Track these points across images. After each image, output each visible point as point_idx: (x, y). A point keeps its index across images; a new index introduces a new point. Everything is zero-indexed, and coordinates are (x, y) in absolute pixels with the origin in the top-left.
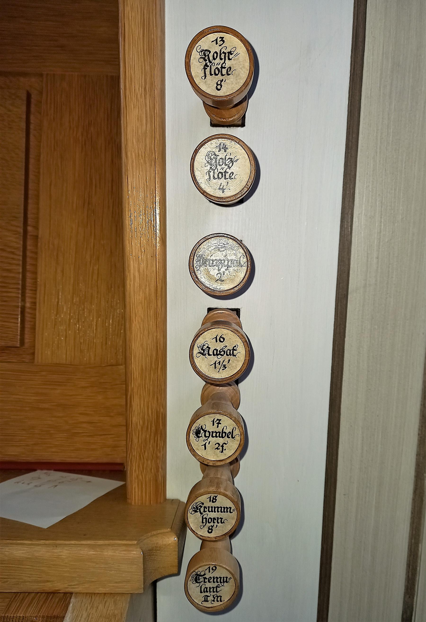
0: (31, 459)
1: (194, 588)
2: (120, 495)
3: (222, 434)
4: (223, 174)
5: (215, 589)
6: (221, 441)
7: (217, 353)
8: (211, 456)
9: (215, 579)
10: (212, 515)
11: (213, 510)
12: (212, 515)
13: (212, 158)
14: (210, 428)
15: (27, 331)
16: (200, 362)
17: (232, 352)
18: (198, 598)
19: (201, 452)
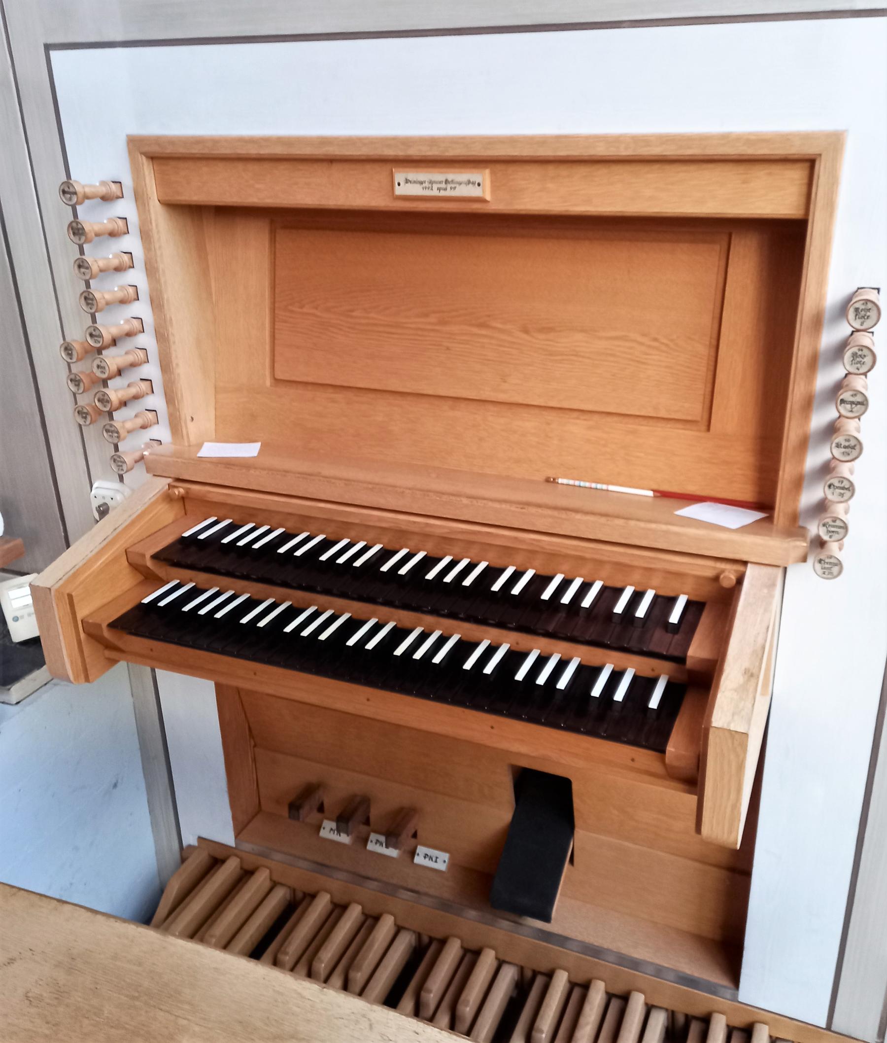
1: (818, 566)
3: (843, 488)
4: (860, 362)
5: (830, 569)
6: (842, 491)
7: (845, 447)
9: (830, 563)
11: (834, 526)
12: (833, 529)
14: (837, 484)
18: (820, 571)
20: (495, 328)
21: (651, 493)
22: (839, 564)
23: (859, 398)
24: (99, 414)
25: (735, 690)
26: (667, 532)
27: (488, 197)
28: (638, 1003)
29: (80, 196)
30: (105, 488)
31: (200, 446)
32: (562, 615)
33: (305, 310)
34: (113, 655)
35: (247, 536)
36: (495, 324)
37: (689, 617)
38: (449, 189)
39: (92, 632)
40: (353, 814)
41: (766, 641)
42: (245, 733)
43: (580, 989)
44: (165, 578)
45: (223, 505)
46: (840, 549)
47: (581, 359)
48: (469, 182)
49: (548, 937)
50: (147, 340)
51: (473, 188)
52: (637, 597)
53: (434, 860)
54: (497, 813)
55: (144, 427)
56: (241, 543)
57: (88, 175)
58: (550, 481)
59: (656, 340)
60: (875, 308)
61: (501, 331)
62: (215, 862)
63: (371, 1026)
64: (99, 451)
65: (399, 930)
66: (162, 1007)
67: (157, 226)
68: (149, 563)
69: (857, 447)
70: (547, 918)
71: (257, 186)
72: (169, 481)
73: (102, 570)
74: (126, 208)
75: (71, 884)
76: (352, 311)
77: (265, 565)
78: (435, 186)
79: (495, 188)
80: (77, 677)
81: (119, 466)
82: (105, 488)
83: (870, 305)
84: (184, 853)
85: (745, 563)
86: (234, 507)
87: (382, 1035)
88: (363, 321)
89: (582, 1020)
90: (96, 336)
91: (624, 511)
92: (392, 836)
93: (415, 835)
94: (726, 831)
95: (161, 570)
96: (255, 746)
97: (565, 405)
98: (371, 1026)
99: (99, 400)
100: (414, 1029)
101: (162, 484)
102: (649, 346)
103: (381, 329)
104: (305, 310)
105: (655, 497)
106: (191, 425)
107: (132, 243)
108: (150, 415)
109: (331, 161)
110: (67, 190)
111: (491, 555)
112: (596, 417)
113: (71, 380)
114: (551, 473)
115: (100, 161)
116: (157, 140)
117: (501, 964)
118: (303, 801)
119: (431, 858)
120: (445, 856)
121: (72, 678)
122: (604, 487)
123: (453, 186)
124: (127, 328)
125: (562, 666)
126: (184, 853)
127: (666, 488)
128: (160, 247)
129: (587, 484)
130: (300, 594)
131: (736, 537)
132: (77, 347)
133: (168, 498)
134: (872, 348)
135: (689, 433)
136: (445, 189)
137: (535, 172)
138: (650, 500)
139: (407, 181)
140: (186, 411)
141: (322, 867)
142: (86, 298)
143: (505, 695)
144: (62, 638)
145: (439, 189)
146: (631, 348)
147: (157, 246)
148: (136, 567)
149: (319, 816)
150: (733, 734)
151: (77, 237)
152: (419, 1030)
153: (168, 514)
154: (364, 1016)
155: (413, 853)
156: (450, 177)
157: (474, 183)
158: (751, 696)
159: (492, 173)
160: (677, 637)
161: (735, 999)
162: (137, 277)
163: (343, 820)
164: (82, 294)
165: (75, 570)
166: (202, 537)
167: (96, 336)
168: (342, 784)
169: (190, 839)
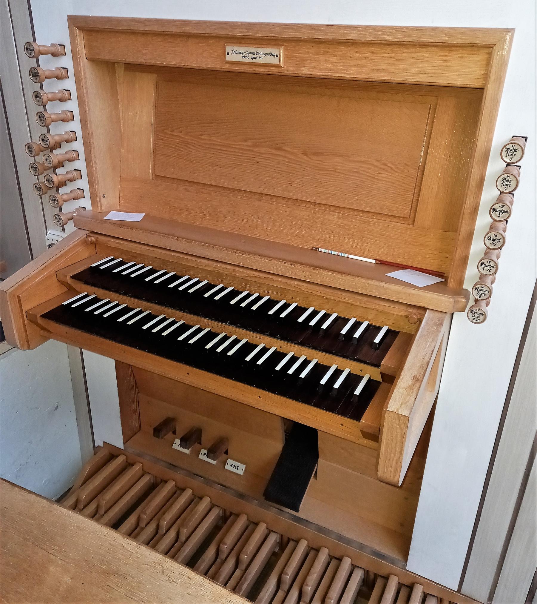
1: (470, 315)
2: (445, 283)
3: (490, 266)
8: (485, 272)
10: (482, 292)
12: (482, 292)
13: (504, 179)
14: (486, 264)
16: (487, 242)
18: (471, 318)
19: (481, 271)
22: (485, 315)
23: (505, 209)
24: (50, 189)
28: (347, 563)
30: (54, 235)
31: (108, 213)
33: (174, 133)
34: (46, 334)
35: (126, 270)
36: (286, 148)
37: (387, 340)
38: (258, 58)
39: (31, 318)
40: (191, 438)
41: (430, 359)
42: (130, 384)
43: (314, 550)
44: (79, 290)
45: (117, 249)
46: (487, 305)
47: (337, 174)
48: (271, 54)
49: (299, 520)
50: (78, 145)
51: (273, 57)
52: (357, 325)
53: (236, 467)
54: (274, 446)
55: (75, 199)
56: (124, 273)
57: (44, 40)
59: (385, 164)
60: (520, 149)
61: (292, 153)
63: (163, 571)
64: (51, 211)
65: (213, 506)
66: (42, 547)
67: (84, 74)
68: (69, 281)
69: (502, 240)
70: (297, 510)
71: (144, 51)
72: (87, 232)
73: (40, 283)
74: (67, 62)
75: (27, 462)
76: (201, 135)
77: (136, 287)
78: (250, 56)
80: (22, 345)
81: (58, 221)
82: (54, 235)
83: (517, 147)
84: (96, 449)
86: (124, 252)
87: (169, 577)
88: (207, 142)
89: (312, 571)
90: (46, 141)
92: (212, 452)
93: (226, 453)
94: (392, 475)
95: (77, 285)
96: (138, 393)
97: (325, 202)
98: (163, 571)
99: (47, 180)
101: (82, 234)
102: (381, 168)
103: (218, 148)
104: (174, 133)
106: (104, 201)
107: (70, 84)
108: (79, 192)
109: (188, 36)
110: (29, 48)
111: (272, 292)
112: (345, 211)
113: (32, 167)
115: (52, 31)
116: (85, 18)
117: (270, 531)
118: (164, 427)
121: (19, 346)
122: (346, 255)
123: (261, 56)
124: (66, 137)
125: (306, 363)
126: (96, 449)
128: (86, 88)
129: (336, 253)
130: (156, 307)
131: (421, 293)
132: (35, 147)
133: (85, 243)
134: (517, 177)
135: (400, 226)
136: (256, 58)
138: (374, 265)
139: (233, 52)
140: (101, 191)
141: (172, 466)
142: (40, 116)
143: (269, 378)
146: (369, 169)
147: (84, 87)
148: (63, 283)
149: (173, 436)
150: (399, 416)
151: (35, 78)
152: (191, 577)
153: (85, 253)
155: (225, 463)
156: (260, 50)
157: (274, 55)
158: (415, 393)
159: (286, 49)
160: (377, 352)
161: (404, 568)
162: (73, 106)
163: (185, 441)
164: (37, 113)
165: (23, 281)
166: (102, 268)
167: (46, 141)
168: (187, 420)
169: (99, 443)
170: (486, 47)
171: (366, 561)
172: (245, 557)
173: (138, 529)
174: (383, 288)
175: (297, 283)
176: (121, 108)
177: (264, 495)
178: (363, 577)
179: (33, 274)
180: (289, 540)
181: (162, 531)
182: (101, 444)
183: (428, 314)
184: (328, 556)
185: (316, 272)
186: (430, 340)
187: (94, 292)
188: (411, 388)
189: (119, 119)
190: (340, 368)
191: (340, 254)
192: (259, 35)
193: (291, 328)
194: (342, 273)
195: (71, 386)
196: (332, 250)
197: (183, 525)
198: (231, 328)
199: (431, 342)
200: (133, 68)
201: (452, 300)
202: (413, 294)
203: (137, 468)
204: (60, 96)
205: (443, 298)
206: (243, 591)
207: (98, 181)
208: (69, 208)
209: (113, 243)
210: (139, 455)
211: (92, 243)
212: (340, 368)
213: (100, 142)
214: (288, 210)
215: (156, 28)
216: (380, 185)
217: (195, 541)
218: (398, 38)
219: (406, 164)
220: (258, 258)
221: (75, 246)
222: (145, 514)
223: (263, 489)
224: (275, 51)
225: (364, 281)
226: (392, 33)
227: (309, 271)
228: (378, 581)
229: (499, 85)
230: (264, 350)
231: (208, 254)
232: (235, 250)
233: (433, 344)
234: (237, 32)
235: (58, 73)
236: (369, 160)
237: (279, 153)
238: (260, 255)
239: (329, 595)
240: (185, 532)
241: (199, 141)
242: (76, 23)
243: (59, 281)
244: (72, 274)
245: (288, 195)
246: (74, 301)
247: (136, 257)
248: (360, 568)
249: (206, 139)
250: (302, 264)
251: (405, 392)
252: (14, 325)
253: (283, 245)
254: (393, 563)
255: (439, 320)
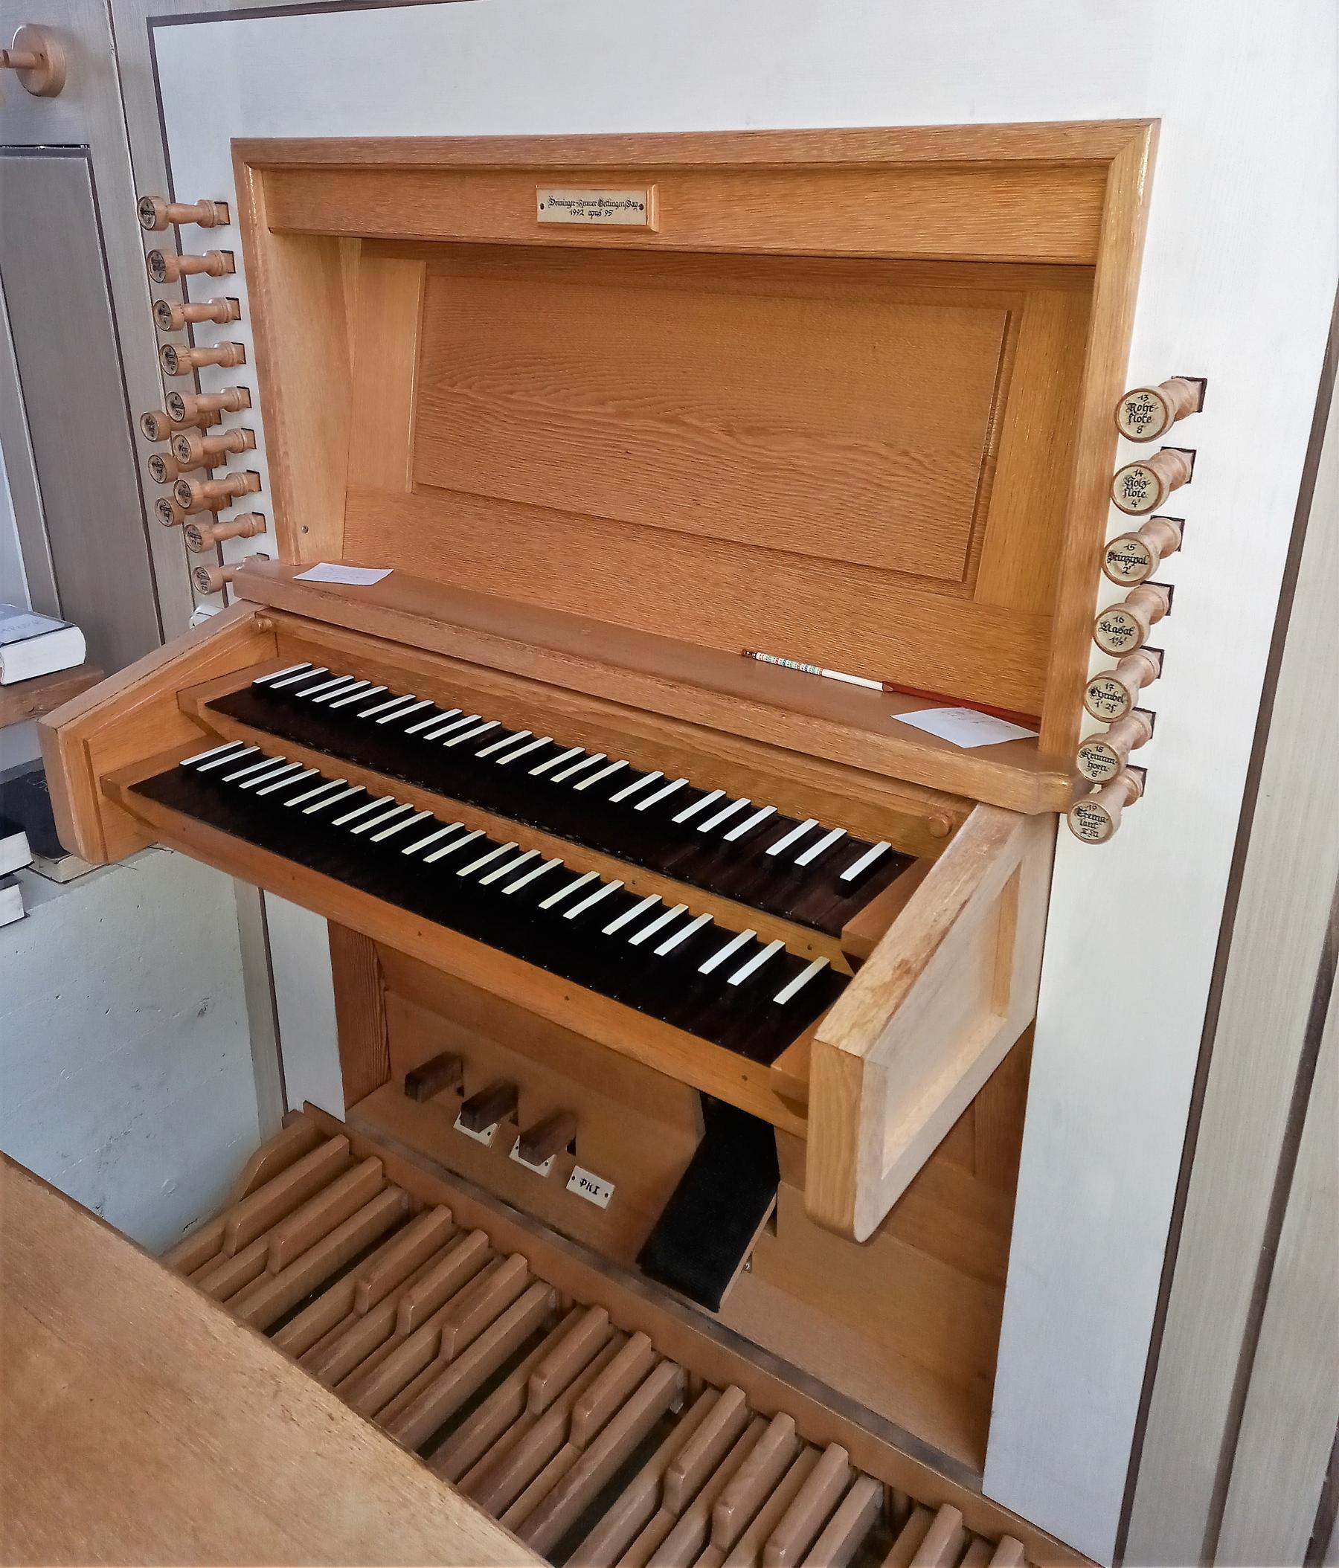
0: (958, 695)
3: (1113, 697)
12: (1098, 762)
14: (1104, 690)
15: (971, 566)
17: (1129, 632)
18: (1078, 829)
20: (684, 424)
21: (879, 686)
25: (873, 990)
26: (862, 742)
27: (654, 227)
29: (160, 216)
32: (693, 849)
33: (456, 390)
35: (322, 694)
38: (586, 213)
39: (110, 789)
42: (360, 969)
48: (629, 204)
50: (252, 418)
51: (634, 211)
54: (679, 1143)
55: (244, 535)
58: (748, 655)
59: (905, 453)
60: (1160, 404)
61: (699, 430)
62: (322, 1137)
63: (276, 1394)
67: (265, 262)
68: (203, 713)
69: (1136, 632)
70: (714, 1307)
71: (378, 209)
73: (138, 714)
74: (230, 238)
76: (511, 393)
77: (344, 732)
79: (664, 214)
84: (289, 1117)
85: (973, 803)
87: (285, 1409)
91: (844, 707)
93: (572, 1149)
95: (225, 724)
96: (386, 989)
97: (774, 544)
98: (276, 1394)
100: (330, 1411)
101: (248, 612)
105: (885, 691)
106: (305, 540)
108: (254, 520)
114: (749, 644)
115: (204, 175)
119: (589, 1187)
120: (609, 1188)
121: (83, 852)
122: (817, 670)
123: (609, 209)
126: (289, 1117)
127: (903, 680)
128: (268, 292)
129: (794, 665)
131: (959, 760)
132: (160, 423)
133: (255, 633)
137: (717, 189)
138: (879, 695)
139: (553, 202)
140: (298, 517)
142: (167, 355)
144: (71, 798)
145: (591, 214)
150: (842, 1055)
152: (336, 1415)
154: (273, 1377)
155: (567, 1176)
156: (606, 196)
158: (892, 1002)
162: (242, 332)
166: (275, 686)
169: (296, 1103)
170: (1091, 165)
171: (890, 1461)
172: (587, 1417)
173: (352, 1316)
174: (877, 747)
175: (683, 729)
176: (351, 336)
177: (638, 1261)
178: (879, 1504)
179: (122, 694)
180: (706, 1385)
181: (404, 1328)
182: (300, 1108)
183: (975, 815)
184: (793, 1439)
185: (725, 704)
186: (965, 877)
187: (257, 740)
188: (887, 988)
189: (347, 361)
190: (753, 940)
191: (802, 667)
192: (601, 161)
193: (655, 838)
194: (784, 708)
195: (238, 965)
196: (808, 663)
197: (453, 1319)
198: (528, 832)
199: (966, 882)
200: (382, 248)
201: (1031, 781)
202: (941, 765)
203: (370, 1170)
204: (214, 310)
205: (1011, 775)
206: (569, 1496)
207: (291, 496)
208: (237, 554)
209: (306, 631)
210: (381, 1141)
211: (265, 631)
212: (753, 940)
213: (299, 409)
214: (692, 562)
215: (397, 158)
216: (896, 503)
217: (475, 1360)
218: (893, 153)
219: (953, 453)
220: (600, 669)
221: (230, 636)
222: (369, 1281)
223: (637, 1246)
224: (637, 196)
225: (829, 727)
226: (882, 144)
227: (709, 703)
228: (913, 1518)
229: (1128, 258)
230: (595, 885)
231: (497, 661)
232: (552, 650)
233: (972, 885)
234: (557, 159)
235: (214, 263)
236: (870, 444)
237: (673, 431)
238: (607, 664)
239: (778, 1535)
240: (454, 1337)
241: (508, 405)
242: (252, 156)
243: (184, 713)
244: (209, 699)
245: (692, 527)
246: (206, 758)
247: (355, 666)
248: (872, 1478)
249: (520, 402)
250: (697, 685)
251: (869, 999)
252: (72, 806)
253: (680, 643)
254: (954, 1476)
255: (998, 831)
